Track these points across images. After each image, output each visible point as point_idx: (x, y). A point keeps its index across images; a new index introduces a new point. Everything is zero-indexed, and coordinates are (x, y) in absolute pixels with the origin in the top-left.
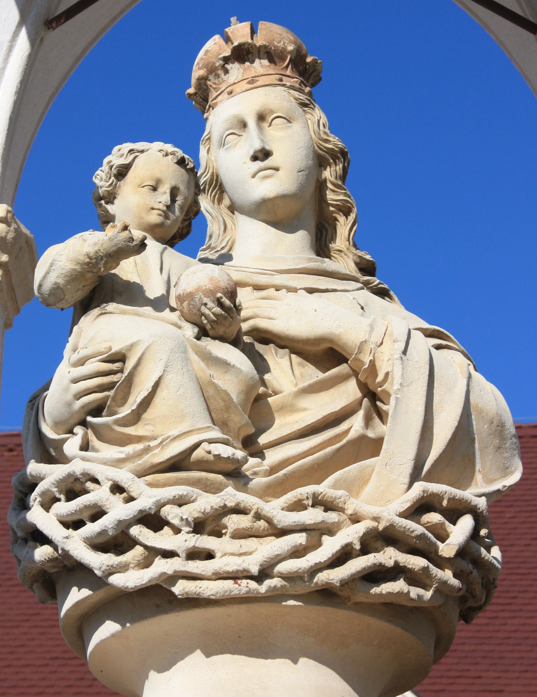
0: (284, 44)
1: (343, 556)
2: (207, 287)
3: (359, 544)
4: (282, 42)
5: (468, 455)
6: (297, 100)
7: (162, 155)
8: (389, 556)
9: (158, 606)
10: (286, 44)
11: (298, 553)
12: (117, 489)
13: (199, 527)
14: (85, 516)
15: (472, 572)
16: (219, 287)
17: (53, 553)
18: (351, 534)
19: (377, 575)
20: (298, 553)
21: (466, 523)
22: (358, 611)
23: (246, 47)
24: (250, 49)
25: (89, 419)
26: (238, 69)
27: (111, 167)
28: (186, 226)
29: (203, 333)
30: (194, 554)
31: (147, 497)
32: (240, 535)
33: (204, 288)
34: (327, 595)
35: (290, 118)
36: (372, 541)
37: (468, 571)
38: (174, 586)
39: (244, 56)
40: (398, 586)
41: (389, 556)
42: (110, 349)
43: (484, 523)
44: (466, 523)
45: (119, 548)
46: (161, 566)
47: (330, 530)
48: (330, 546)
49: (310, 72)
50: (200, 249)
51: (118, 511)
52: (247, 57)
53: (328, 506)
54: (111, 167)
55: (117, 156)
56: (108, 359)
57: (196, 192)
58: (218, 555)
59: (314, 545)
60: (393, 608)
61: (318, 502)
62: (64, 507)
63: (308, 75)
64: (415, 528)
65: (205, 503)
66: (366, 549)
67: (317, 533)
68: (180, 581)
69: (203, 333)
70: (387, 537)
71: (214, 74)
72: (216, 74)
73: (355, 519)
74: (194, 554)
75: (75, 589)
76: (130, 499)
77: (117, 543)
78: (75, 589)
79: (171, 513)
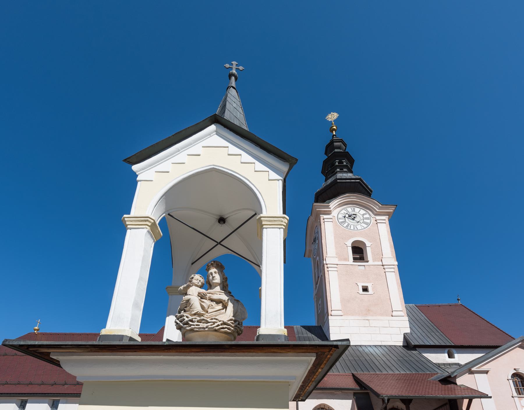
1: (218, 325)
8: (225, 326)
11: (211, 325)
12: (187, 317)
13: (198, 322)
17: (455, 394)
18: (220, 323)
20: (211, 325)
29: (202, 298)
30: (197, 325)
31: (190, 318)
34: (216, 330)
36: (221, 325)
38: (104, 327)
40: (226, 329)
41: (225, 326)
46: (193, 327)
47: (216, 322)
48: (216, 324)
51: (186, 319)
53: (217, 319)
55: (192, 276)
60: (226, 333)
61: (215, 319)
64: (229, 322)
65: (198, 318)
66: (221, 325)
67: (214, 323)
68: (194, 287)
69: (202, 298)
70: (224, 323)
74: (197, 325)
77: (187, 323)
79: (194, 320)
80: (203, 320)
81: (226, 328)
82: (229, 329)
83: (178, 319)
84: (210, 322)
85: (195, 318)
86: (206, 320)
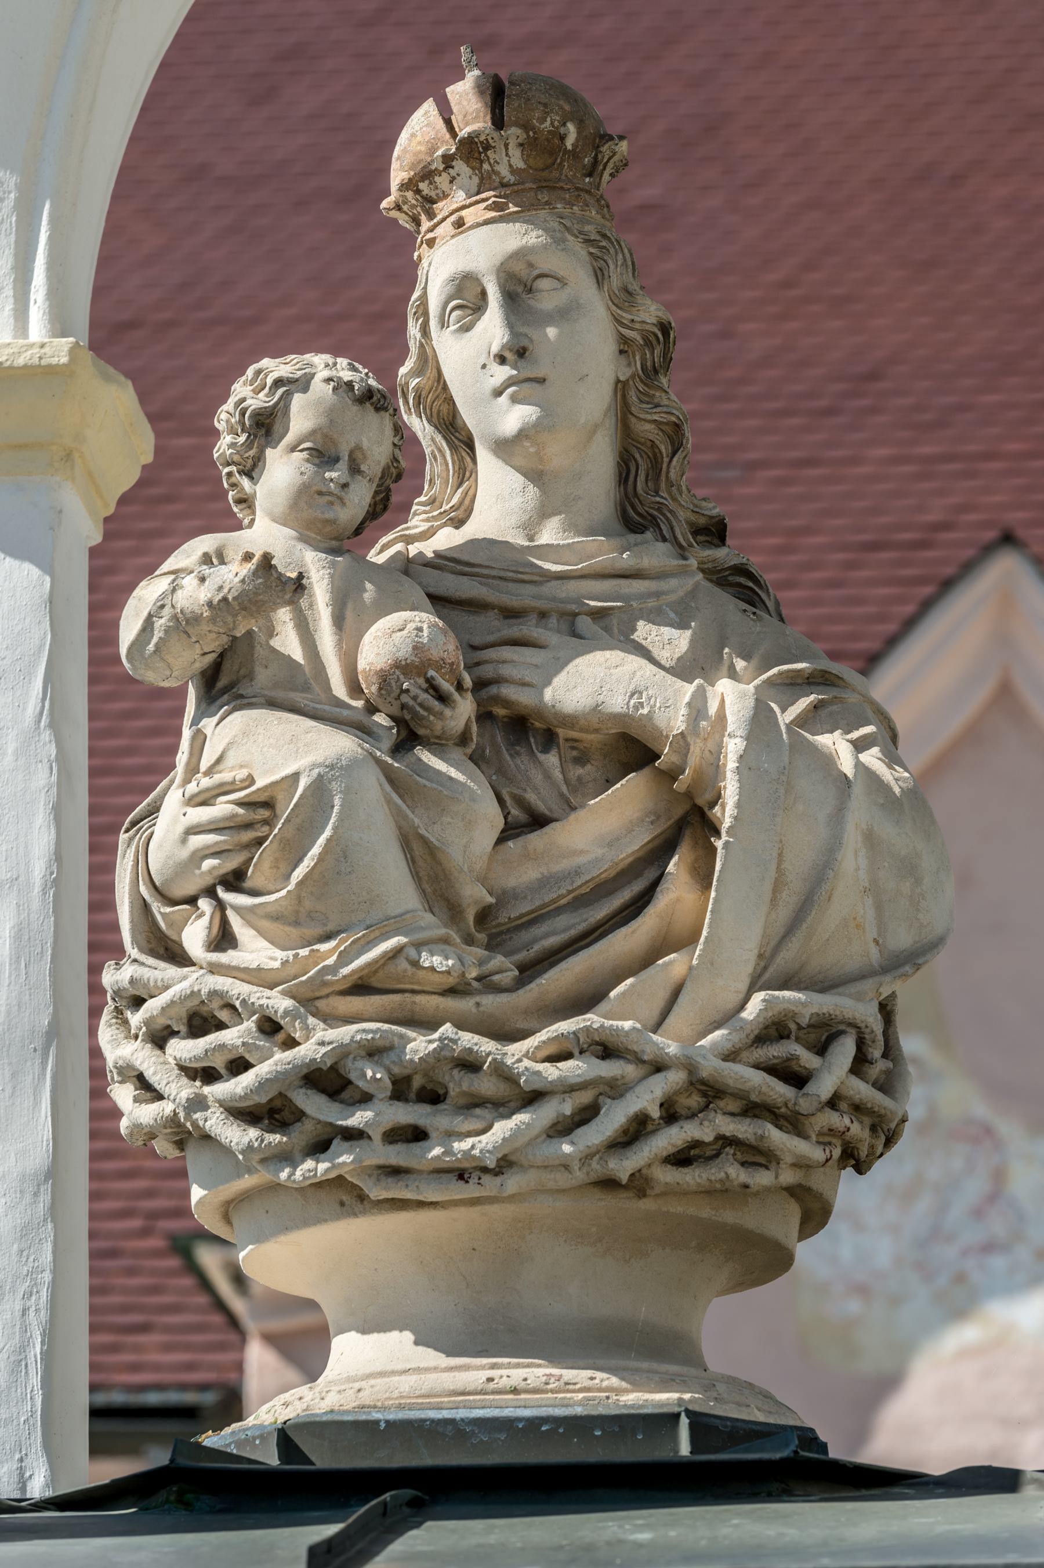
0: (552, 124)
2: (409, 661)
3: (657, 1108)
4: (549, 119)
5: (855, 919)
6: (577, 237)
7: (331, 387)
9: (342, 1204)
10: (556, 123)
11: (563, 1129)
13: (401, 1090)
14: (219, 1063)
15: (849, 1129)
16: (430, 660)
18: (647, 1098)
20: (563, 1129)
21: (845, 1050)
23: (482, 138)
24: (491, 141)
25: (221, 892)
26: (470, 177)
27: (243, 413)
28: (382, 500)
31: (318, 1041)
32: (474, 1103)
33: (403, 663)
37: (842, 1129)
39: (480, 153)
42: (251, 780)
43: (873, 1042)
44: (845, 1050)
45: (277, 1116)
47: (616, 1089)
48: (614, 1119)
49: (605, 160)
50: (416, 501)
51: (273, 1063)
52: (486, 155)
54: (243, 413)
56: (247, 800)
57: (396, 442)
58: (433, 1135)
59: (587, 1115)
62: (183, 1048)
63: (601, 167)
64: (749, 1077)
66: (671, 1115)
71: (427, 182)
72: (431, 183)
73: (658, 1067)
75: (276, 643)
76: (291, 1043)
78: (276, 643)
80: (470, 1064)
81: (725, 1141)
83: (159, 1039)
84: (533, 1098)
85: (374, 1052)
86: (504, 1073)
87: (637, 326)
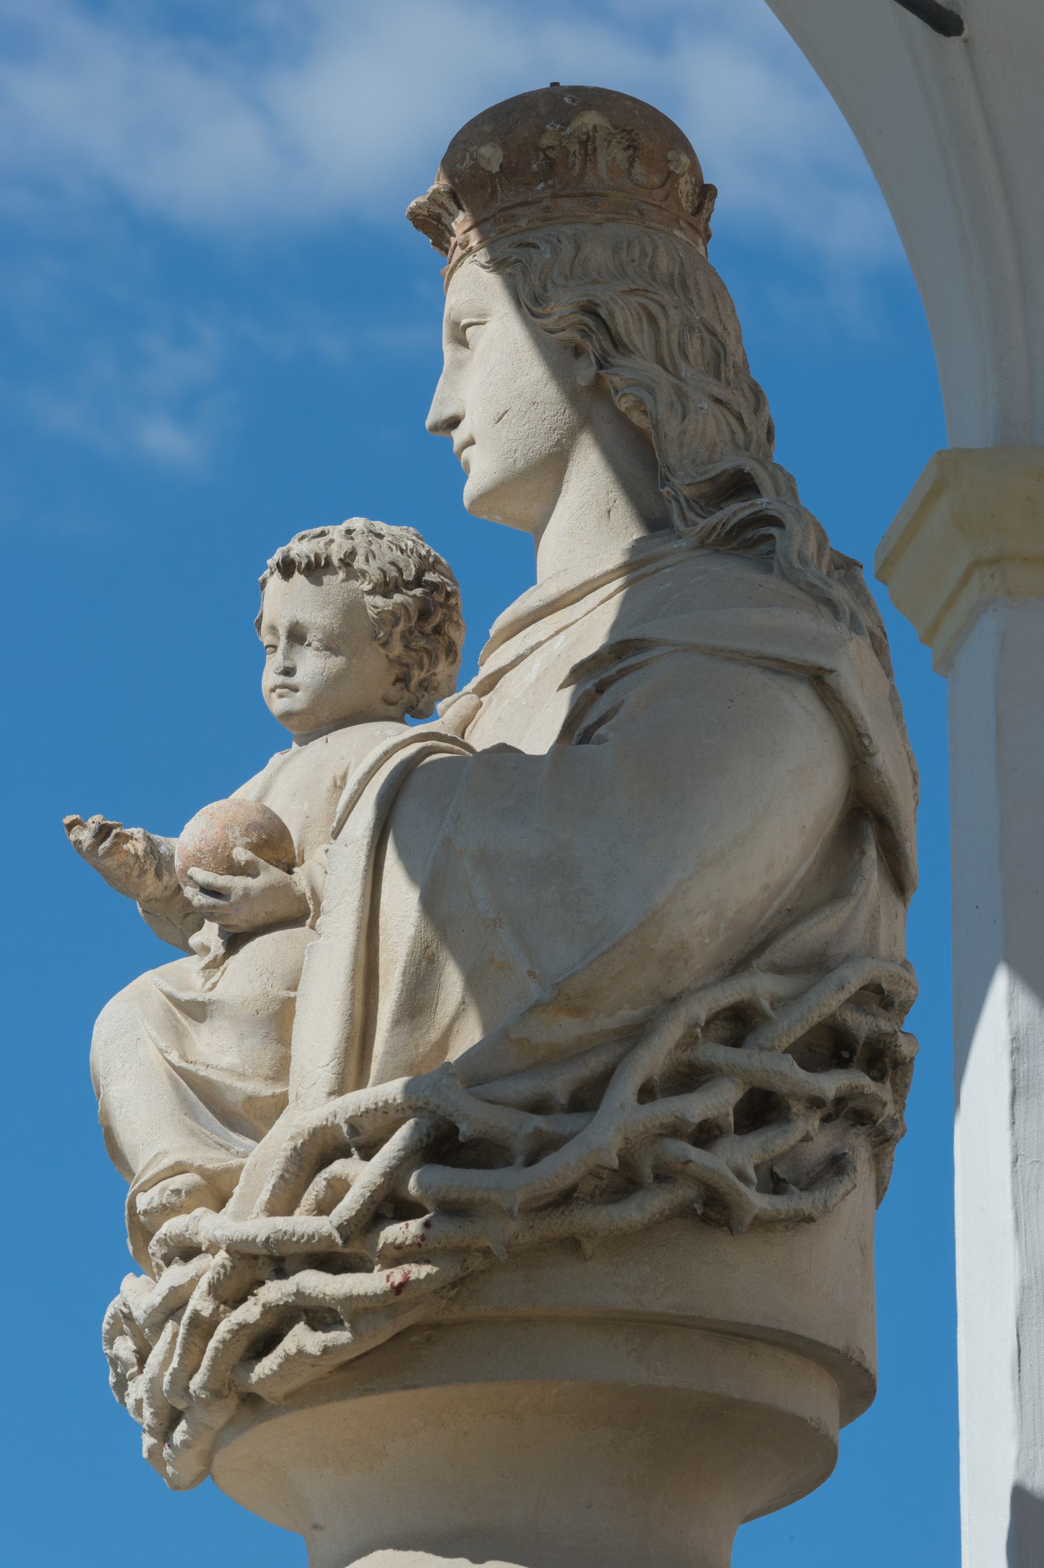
4: (468, 156)
5: (492, 960)
19: (263, 1340)
22: (301, 1407)
35: (479, 316)
36: (230, 1293)
82: (320, 1315)
87: (563, 324)
